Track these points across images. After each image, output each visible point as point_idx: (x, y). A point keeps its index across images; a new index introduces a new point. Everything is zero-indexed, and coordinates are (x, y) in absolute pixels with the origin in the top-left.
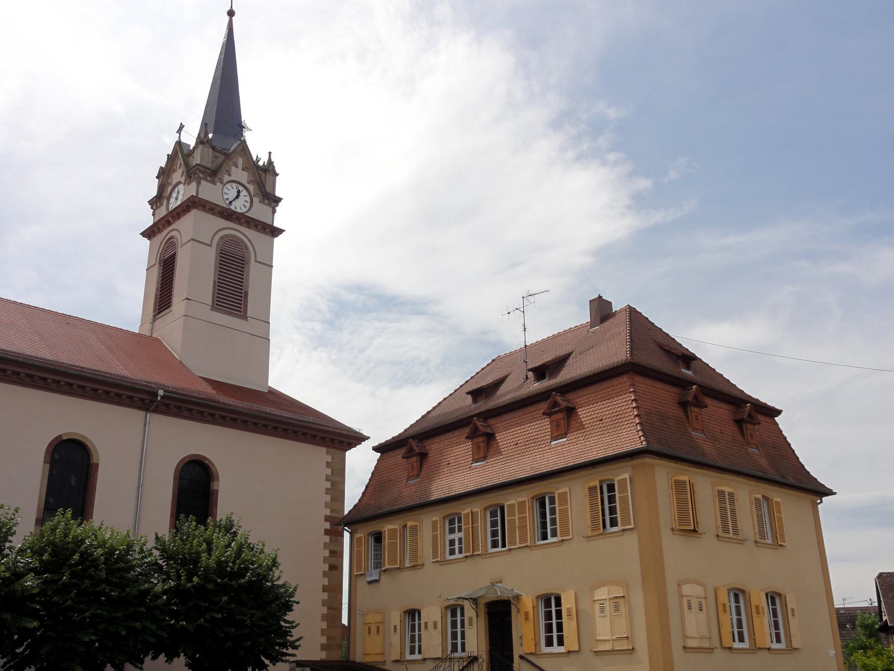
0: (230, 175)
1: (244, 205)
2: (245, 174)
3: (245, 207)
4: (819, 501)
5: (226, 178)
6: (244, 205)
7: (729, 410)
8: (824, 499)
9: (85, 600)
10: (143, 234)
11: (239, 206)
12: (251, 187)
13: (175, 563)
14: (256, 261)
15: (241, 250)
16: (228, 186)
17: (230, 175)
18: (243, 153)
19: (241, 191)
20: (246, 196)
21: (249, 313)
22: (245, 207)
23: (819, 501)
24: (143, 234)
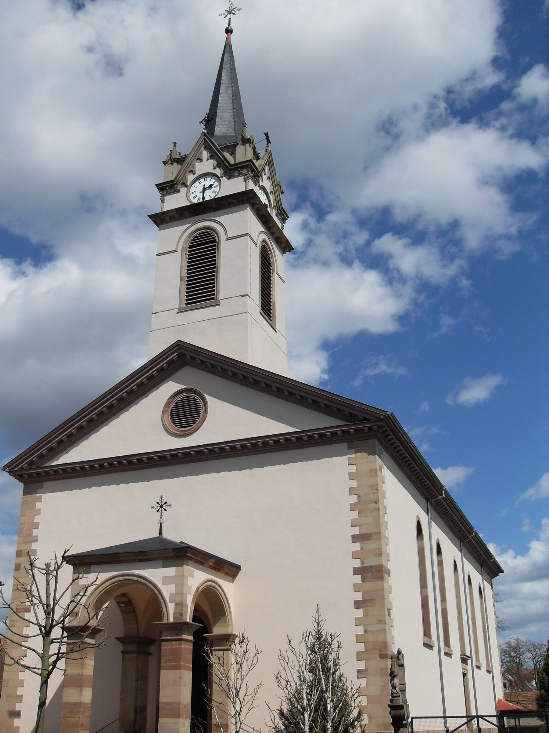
0: (194, 174)
5: (191, 178)
14: (228, 239)
17: (194, 174)
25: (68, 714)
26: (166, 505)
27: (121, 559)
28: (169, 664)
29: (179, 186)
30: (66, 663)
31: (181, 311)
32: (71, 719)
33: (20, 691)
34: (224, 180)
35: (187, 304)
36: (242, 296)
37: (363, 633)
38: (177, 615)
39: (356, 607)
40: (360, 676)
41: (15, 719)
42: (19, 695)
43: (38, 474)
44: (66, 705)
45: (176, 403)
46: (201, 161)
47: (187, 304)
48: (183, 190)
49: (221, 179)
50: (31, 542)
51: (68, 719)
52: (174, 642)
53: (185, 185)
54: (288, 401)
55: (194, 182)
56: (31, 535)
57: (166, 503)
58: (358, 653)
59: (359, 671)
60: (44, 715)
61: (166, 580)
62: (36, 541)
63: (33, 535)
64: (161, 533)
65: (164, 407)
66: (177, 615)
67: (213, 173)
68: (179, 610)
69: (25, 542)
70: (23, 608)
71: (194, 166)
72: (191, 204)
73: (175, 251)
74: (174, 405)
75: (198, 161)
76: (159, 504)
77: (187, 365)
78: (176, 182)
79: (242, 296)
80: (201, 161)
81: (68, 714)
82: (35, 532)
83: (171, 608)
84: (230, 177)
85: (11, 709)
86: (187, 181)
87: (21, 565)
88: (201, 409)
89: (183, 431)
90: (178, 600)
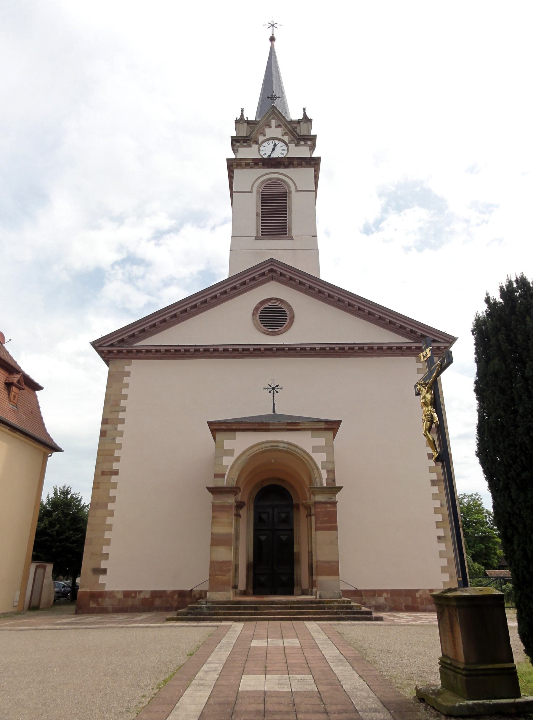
0: (265, 136)
1: (282, 150)
2: (280, 130)
3: (284, 150)
4: (50, 455)
5: (261, 138)
6: (282, 150)
7: (484, 317)
8: (54, 454)
9: (54, 550)
10: (210, 424)
11: (279, 153)
12: (286, 139)
13: (472, 524)
14: (297, 191)
15: (281, 185)
16: (265, 144)
17: (265, 136)
18: (275, 116)
19: (277, 144)
20: (283, 146)
21: (294, 233)
22: (284, 150)
23: (50, 455)
24: (210, 424)
25: (218, 573)
26: (277, 387)
27: (271, 427)
28: (324, 525)
29: (251, 143)
30: (212, 523)
31: (257, 238)
32: (220, 577)
33: (105, 549)
34: (292, 146)
35: (262, 235)
36: (313, 236)
37: (440, 506)
38: (330, 481)
39: (432, 485)
40: (440, 541)
41: (100, 576)
42: (104, 553)
43: (129, 352)
44: (215, 563)
45: (263, 309)
46: (270, 127)
47: (262, 235)
48: (255, 146)
49: (289, 145)
50: (118, 411)
51: (217, 576)
52: (328, 505)
53: (256, 142)
54: (364, 320)
55: (263, 142)
56: (118, 405)
57: (277, 386)
58: (437, 522)
59: (439, 538)
60: (297, 576)
61: (316, 449)
62: (124, 411)
63: (121, 406)
64: (274, 411)
65: (254, 310)
66: (330, 481)
67: (281, 139)
68: (331, 476)
69: (111, 412)
70: (109, 472)
71: (264, 130)
72: (261, 157)
73: (251, 192)
74: (262, 311)
75: (268, 127)
76: (276, 387)
77: (273, 280)
78: (249, 138)
79: (313, 236)
80: (270, 127)
81: (218, 573)
82: (123, 403)
83: (324, 473)
84: (297, 145)
85: (95, 567)
86: (258, 140)
87: (107, 432)
88: (287, 317)
89: (271, 332)
90: (330, 467)
